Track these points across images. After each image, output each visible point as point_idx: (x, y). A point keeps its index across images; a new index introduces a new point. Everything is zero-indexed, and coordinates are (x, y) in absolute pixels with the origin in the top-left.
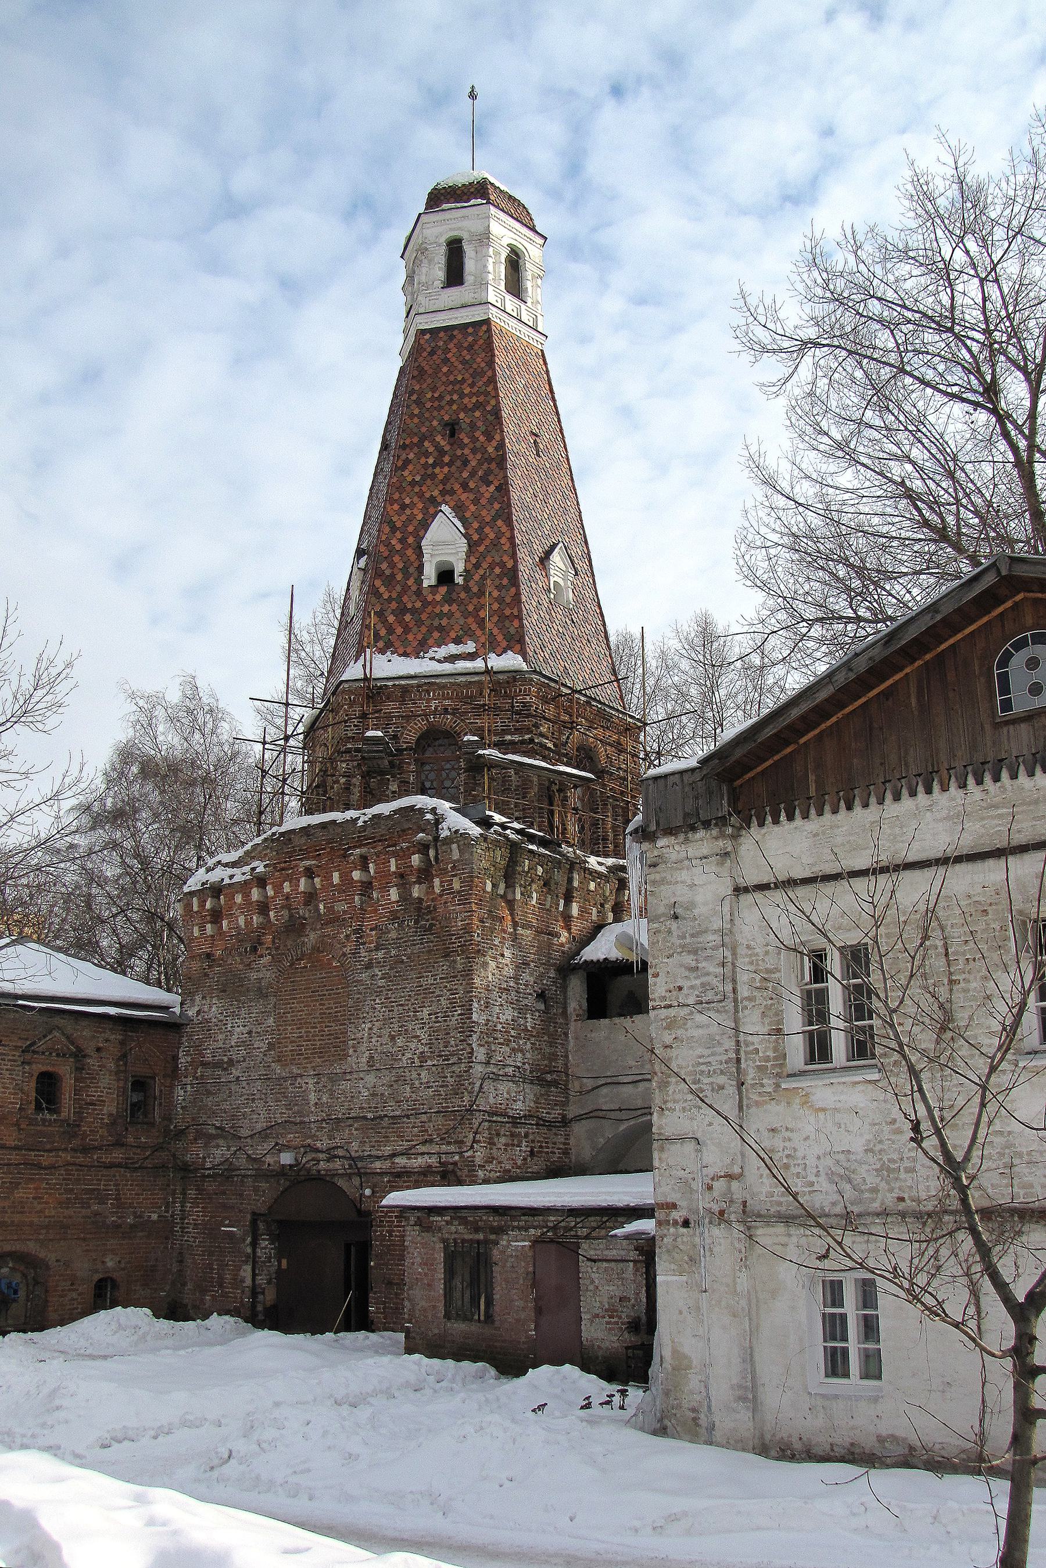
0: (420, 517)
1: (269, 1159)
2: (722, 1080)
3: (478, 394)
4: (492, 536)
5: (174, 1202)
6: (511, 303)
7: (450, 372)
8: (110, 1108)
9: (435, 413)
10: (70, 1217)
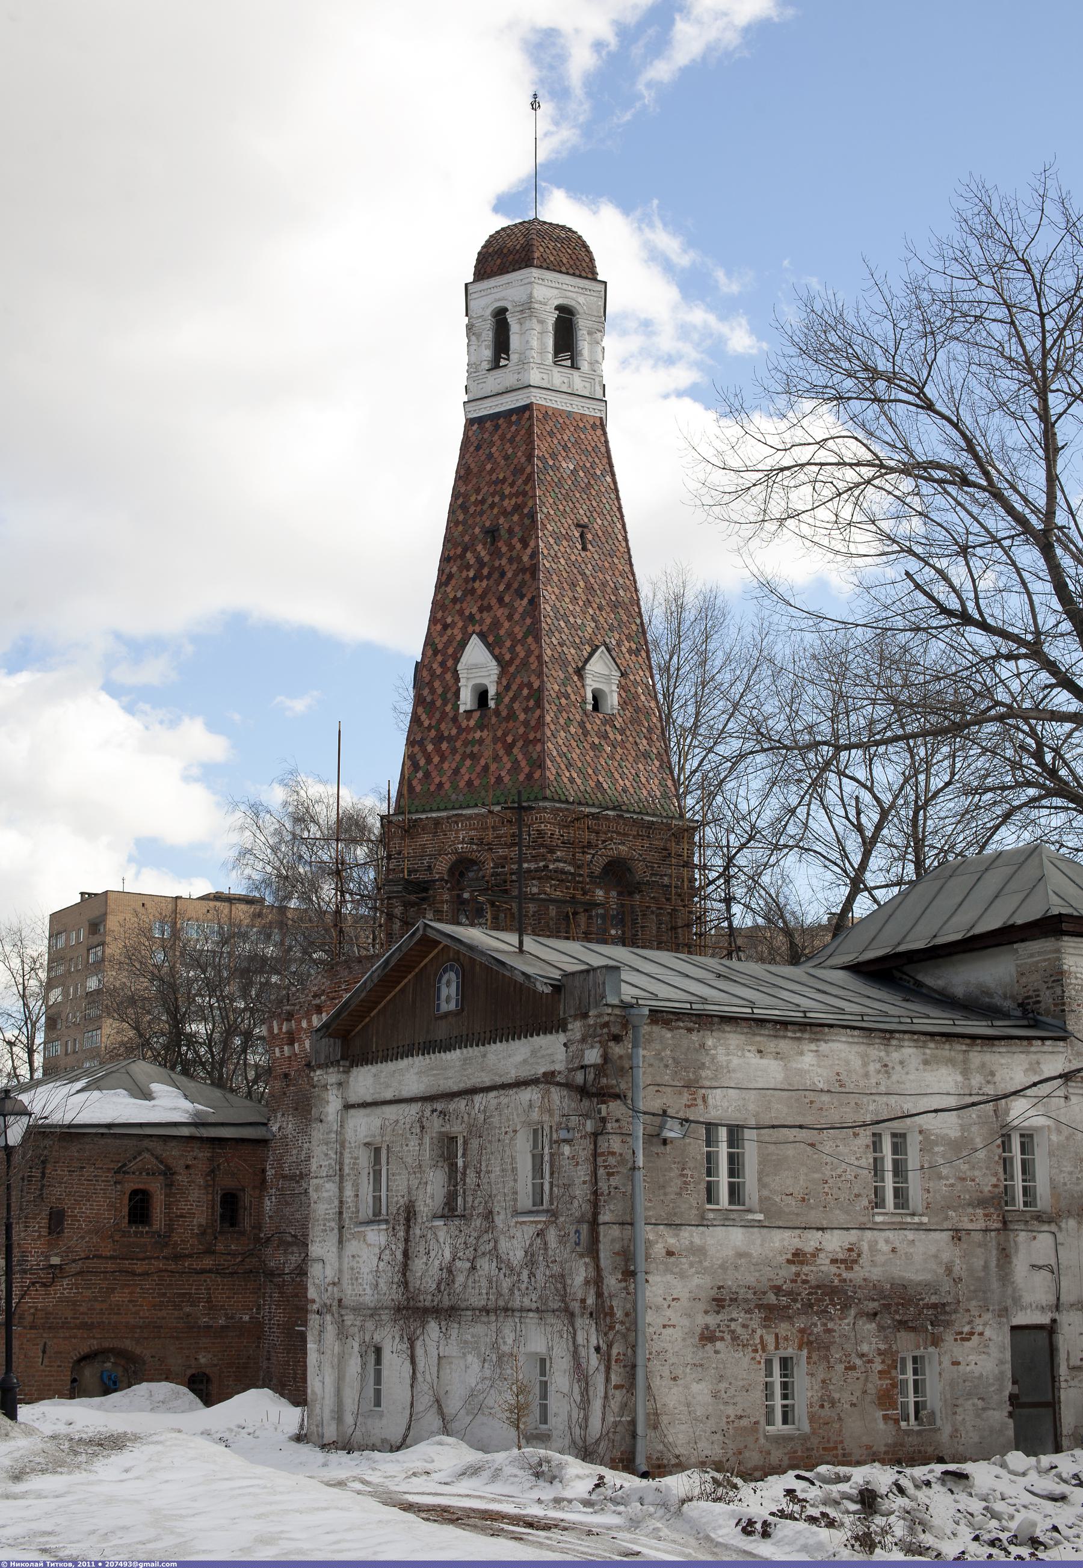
0: (459, 638)
3: (517, 495)
4: (522, 654)
5: (264, 1305)
6: (559, 377)
7: (493, 470)
9: (478, 519)
10: (164, 1318)
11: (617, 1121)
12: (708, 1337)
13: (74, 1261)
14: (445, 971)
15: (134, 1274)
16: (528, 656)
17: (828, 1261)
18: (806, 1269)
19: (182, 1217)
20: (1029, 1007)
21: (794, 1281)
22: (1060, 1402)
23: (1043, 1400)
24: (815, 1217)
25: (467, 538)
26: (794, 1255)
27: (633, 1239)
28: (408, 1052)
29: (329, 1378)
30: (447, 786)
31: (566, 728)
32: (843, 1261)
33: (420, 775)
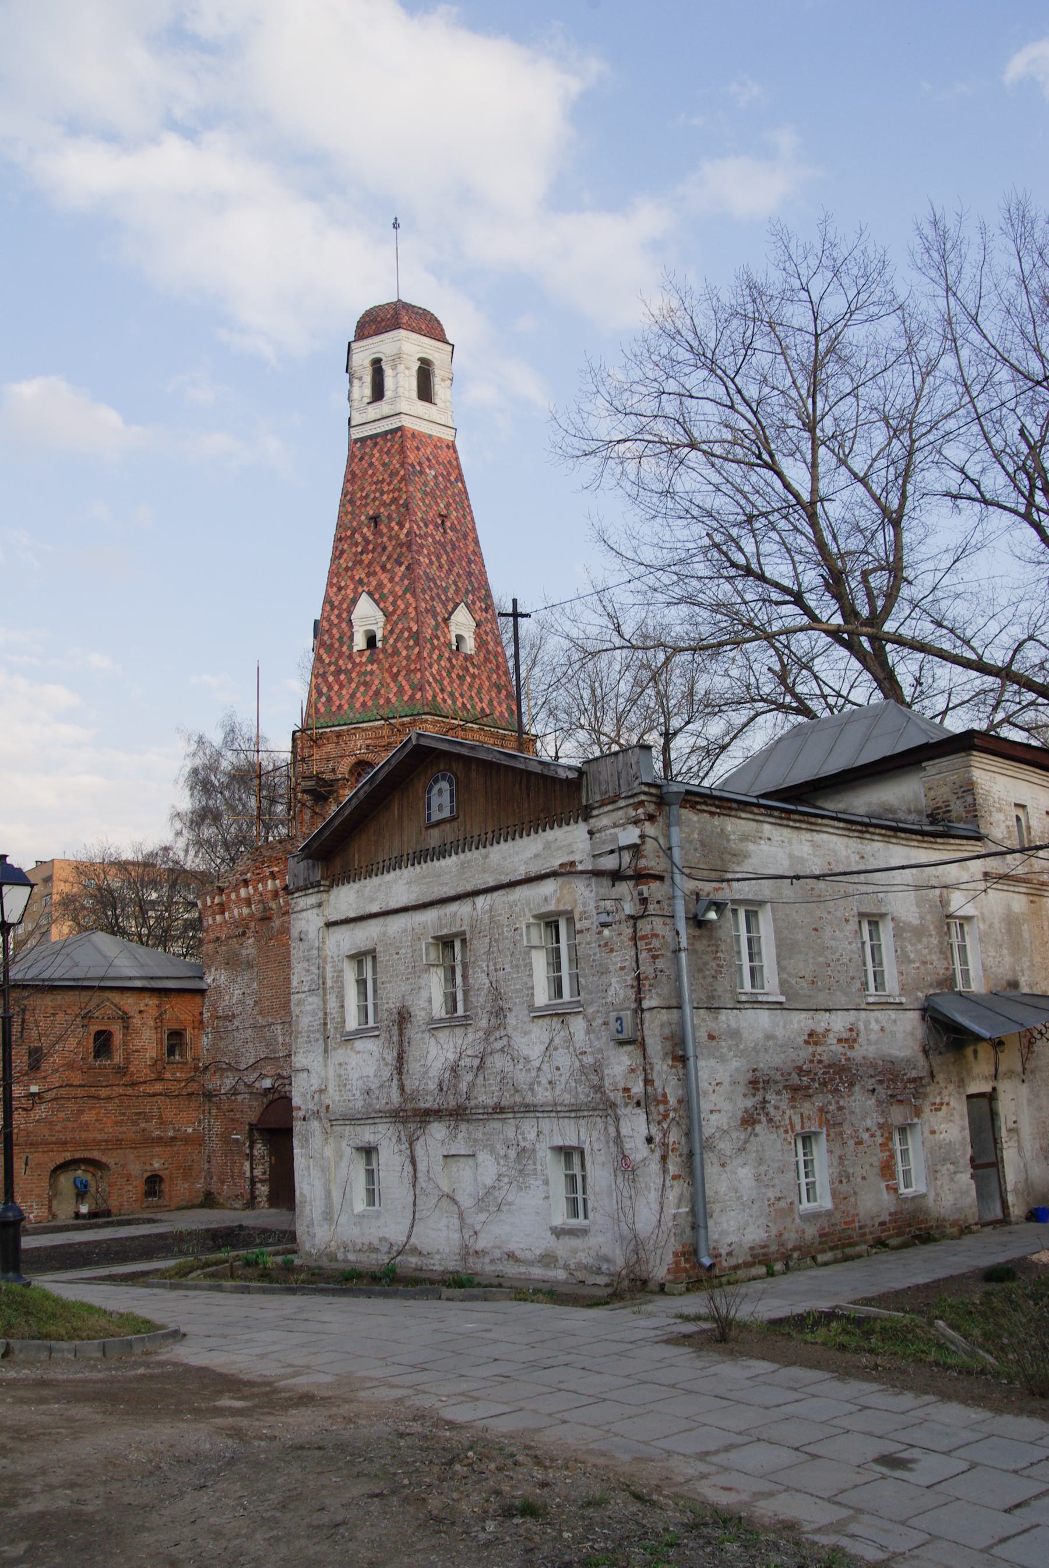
0: (351, 596)
1: (257, 1085)
2: (318, 1035)
3: (393, 491)
4: (402, 607)
6: (421, 408)
7: (374, 474)
8: (151, 1053)
9: (363, 510)
11: (658, 902)
12: (749, 1121)
13: (50, 1090)
14: (436, 781)
15: (98, 1098)
16: (407, 608)
17: (835, 1041)
18: (819, 1049)
19: (137, 1051)
20: (939, 817)
21: (812, 1061)
22: (1002, 1161)
23: (990, 1161)
24: (822, 999)
25: (355, 524)
26: (810, 1035)
27: (682, 1024)
28: (396, 864)
29: (318, 1184)
30: (346, 707)
31: (438, 662)
32: (847, 1040)
33: (323, 699)
